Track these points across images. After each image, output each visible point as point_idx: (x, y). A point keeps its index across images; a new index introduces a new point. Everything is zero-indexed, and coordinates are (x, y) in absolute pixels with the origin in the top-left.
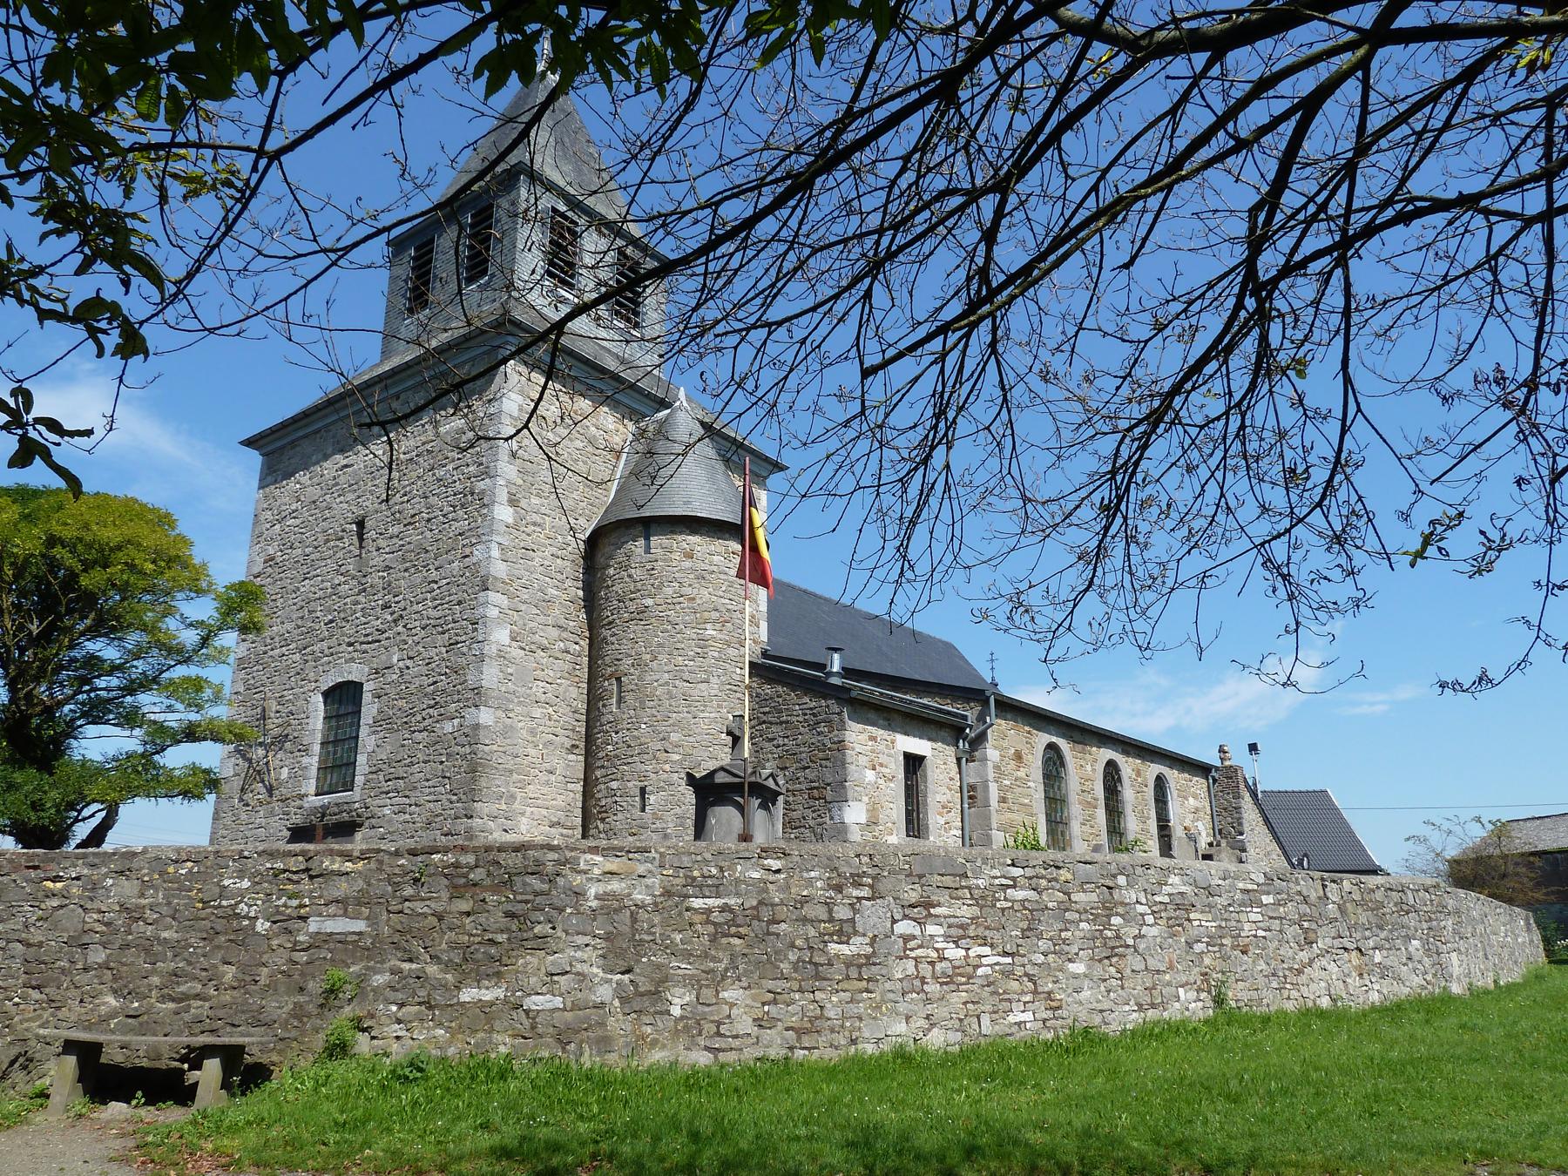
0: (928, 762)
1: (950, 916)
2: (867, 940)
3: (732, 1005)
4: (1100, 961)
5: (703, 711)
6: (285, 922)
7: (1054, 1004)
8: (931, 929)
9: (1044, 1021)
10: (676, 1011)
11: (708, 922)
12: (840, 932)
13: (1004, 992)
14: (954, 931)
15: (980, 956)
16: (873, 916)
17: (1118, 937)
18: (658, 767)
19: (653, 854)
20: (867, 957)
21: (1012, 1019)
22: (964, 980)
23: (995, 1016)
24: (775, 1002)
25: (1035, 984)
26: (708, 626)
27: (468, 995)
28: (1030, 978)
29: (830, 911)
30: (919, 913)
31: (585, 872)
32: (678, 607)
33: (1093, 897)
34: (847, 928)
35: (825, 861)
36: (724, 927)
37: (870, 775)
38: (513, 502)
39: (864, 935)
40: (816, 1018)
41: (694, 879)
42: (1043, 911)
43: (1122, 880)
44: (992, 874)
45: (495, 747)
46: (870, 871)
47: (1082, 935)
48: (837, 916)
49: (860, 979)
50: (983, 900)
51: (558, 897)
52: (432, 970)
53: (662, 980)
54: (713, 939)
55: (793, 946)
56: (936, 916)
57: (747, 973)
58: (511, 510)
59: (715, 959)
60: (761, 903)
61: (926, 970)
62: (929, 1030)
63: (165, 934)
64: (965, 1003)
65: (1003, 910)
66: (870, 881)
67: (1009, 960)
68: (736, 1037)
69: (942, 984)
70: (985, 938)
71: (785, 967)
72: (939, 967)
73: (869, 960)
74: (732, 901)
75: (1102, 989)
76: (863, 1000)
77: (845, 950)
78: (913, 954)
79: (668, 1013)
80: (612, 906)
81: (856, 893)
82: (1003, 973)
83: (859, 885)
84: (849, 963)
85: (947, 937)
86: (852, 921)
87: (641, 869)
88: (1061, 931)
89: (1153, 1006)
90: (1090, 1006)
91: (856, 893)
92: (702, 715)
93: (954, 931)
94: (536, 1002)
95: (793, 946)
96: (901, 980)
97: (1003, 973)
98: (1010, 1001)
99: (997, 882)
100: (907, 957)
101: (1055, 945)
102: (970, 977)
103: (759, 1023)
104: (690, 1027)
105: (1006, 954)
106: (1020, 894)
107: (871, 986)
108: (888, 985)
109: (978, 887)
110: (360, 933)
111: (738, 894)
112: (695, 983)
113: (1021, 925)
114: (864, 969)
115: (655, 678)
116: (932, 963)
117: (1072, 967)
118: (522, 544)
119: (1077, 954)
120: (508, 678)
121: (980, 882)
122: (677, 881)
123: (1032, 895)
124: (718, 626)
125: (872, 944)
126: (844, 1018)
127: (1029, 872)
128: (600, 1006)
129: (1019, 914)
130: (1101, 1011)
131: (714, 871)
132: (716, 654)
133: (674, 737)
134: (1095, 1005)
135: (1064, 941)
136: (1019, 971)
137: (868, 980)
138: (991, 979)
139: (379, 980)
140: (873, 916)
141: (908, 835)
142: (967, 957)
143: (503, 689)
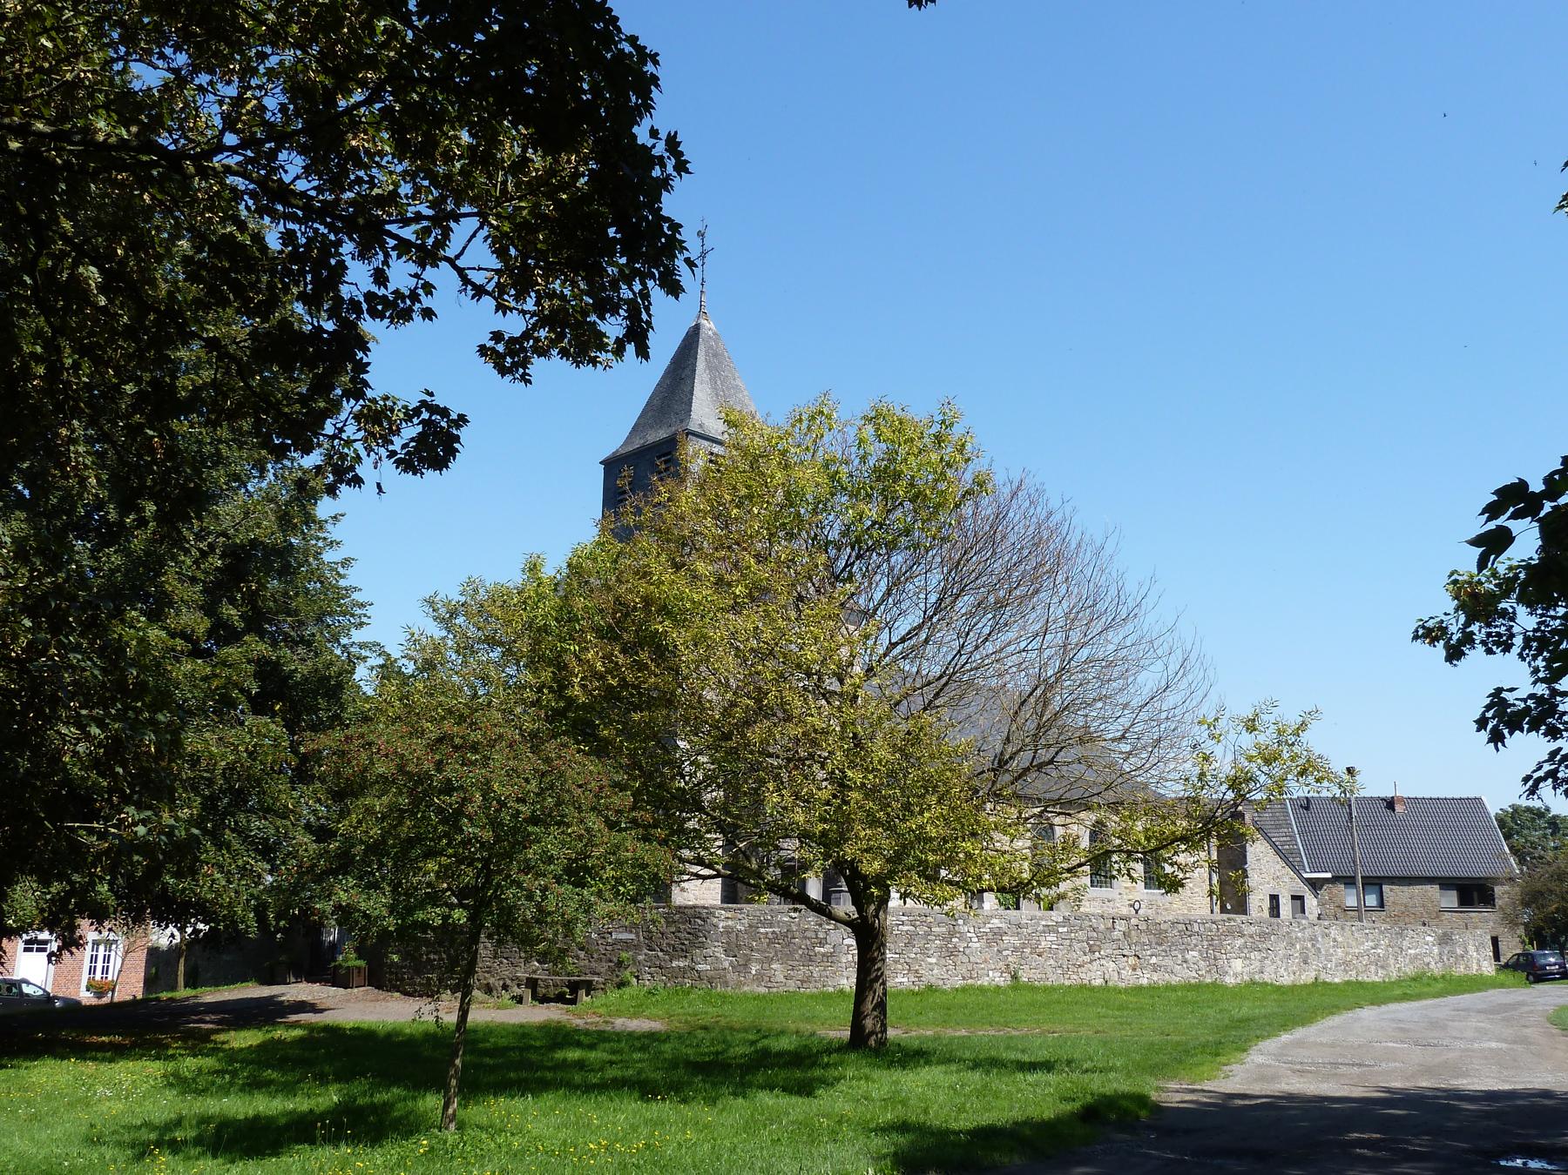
21: (897, 980)
43: (961, 922)
52: (660, 954)
53: (748, 960)
71: (797, 956)
77: (822, 949)
80: (728, 931)
84: (823, 955)
89: (971, 978)
94: (700, 967)
104: (759, 978)
106: (905, 928)
117: (929, 960)
123: (912, 928)
127: (911, 918)
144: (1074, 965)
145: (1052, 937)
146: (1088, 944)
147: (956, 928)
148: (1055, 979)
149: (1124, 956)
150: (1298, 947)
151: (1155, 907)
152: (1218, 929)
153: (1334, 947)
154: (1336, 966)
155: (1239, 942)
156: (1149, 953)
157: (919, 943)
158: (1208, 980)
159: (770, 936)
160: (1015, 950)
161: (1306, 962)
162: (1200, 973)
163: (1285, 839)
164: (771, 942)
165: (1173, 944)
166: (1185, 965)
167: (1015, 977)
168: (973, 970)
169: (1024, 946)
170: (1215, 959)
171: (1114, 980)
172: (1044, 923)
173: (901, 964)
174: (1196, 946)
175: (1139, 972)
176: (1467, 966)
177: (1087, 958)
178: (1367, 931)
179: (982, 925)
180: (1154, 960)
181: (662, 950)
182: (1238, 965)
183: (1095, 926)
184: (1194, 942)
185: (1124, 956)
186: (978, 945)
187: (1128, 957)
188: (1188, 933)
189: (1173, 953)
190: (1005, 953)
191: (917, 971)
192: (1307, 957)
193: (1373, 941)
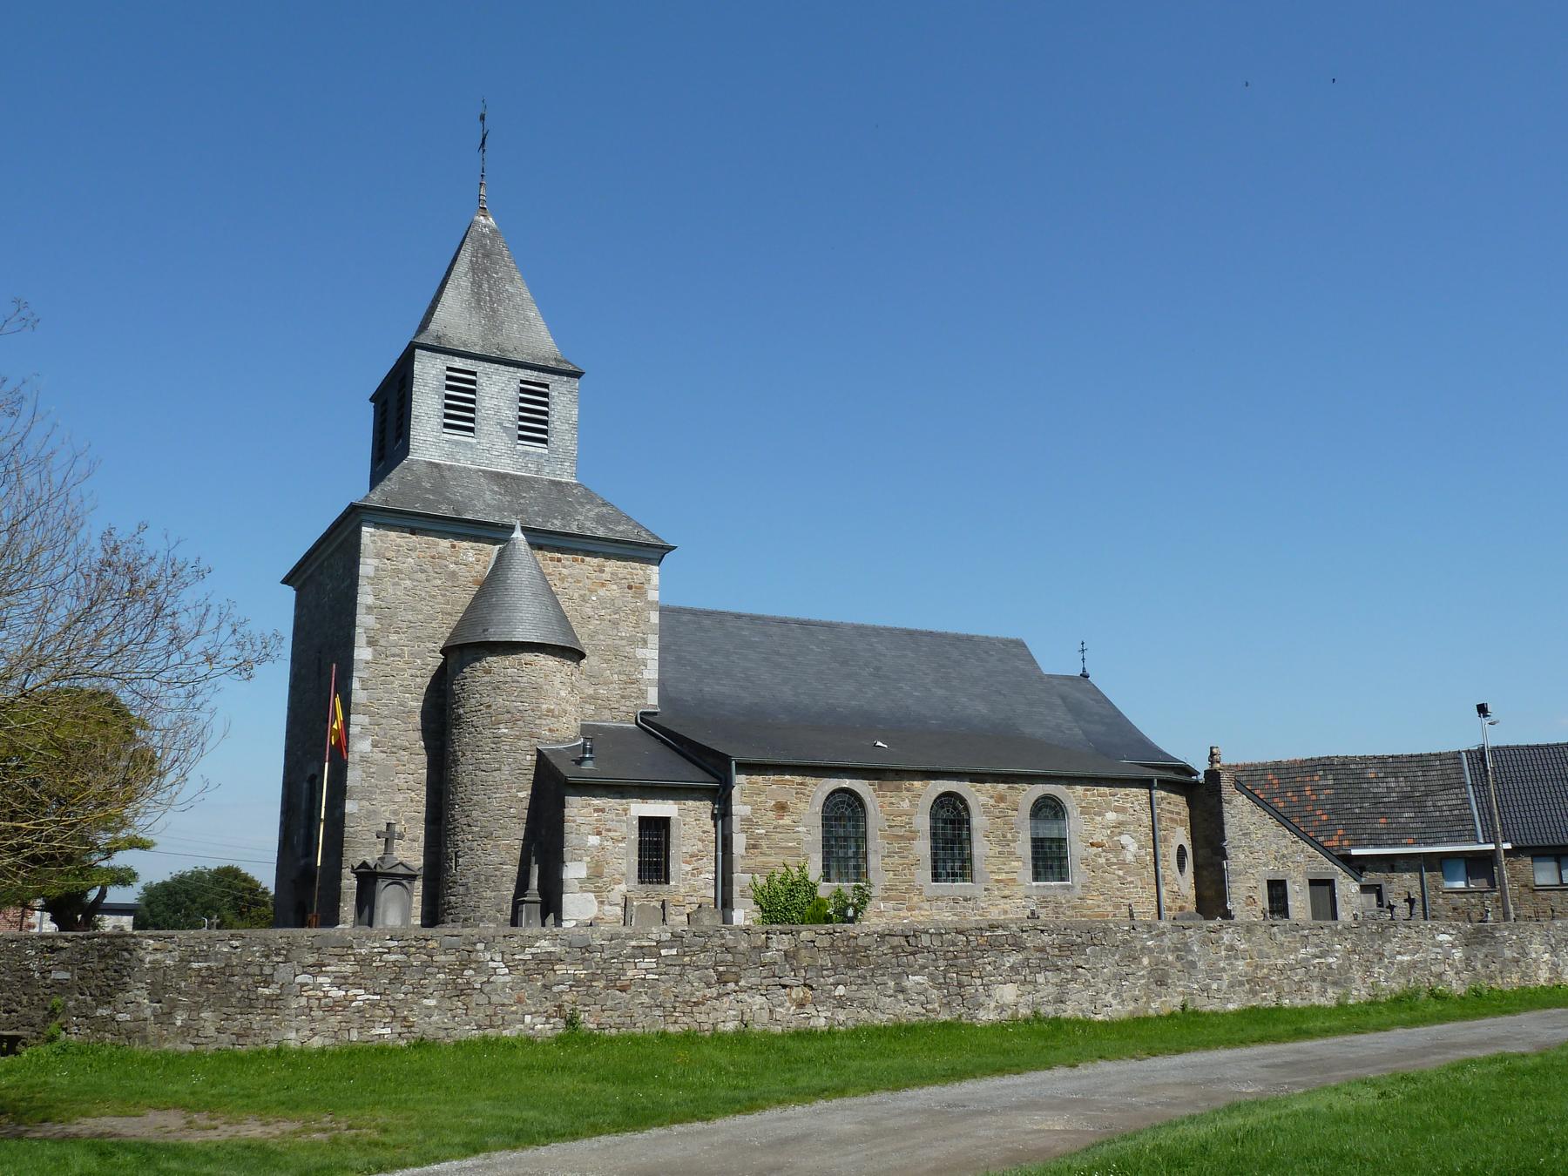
0: (672, 822)
1: (336, 972)
2: (279, 986)
3: (205, 1020)
4: (449, 998)
5: (495, 793)
6: (45, 973)
7: (408, 1024)
8: (320, 980)
9: (400, 1034)
10: (179, 1023)
11: (199, 975)
12: (265, 981)
13: (371, 1016)
14: (337, 981)
15: (356, 995)
16: (283, 973)
17: (468, 983)
18: (464, 837)
19: (176, 939)
20: (277, 995)
21: (374, 1032)
22: (340, 1009)
23: (360, 1030)
24: (227, 1019)
25: (394, 1012)
26: (501, 726)
27: (100, 1012)
28: (392, 1008)
29: (262, 970)
30: (313, 970)
31: (145, 949)
32: (479, 713)
33: (453, 958)
34: (269, 979)
35: (263, 941)
36: (205, 979)
37: (594, 840)
38: (371, 643)
39: (277, 983)
40: (248, 1029)
41: (195, 952)
42: (409, 967)
43: (480, 946)
44: (373, 945)
45: (360, 828)
46: (286, 946)
47: (437, 982)
48: (264, 972)
49: (272, 1008)
50: (363, 962)
51: (133, 963)
52: (89, 999)
53: (174, 1007)
54: (200, 985)
55: (240, 989)
56: (325, 972)
57: (214, 1004)
58: (370, 649)
59: (199, 996)
60: (226, 965)
61: (314, 1003)
62: (312, 1037)
63: (6, 979)
64: (340, 1022)
65: (377, 967)
66: (285, 952)
67: (378, 997)
68: (206, 1037)
69: (324, 1011)
70: (361, 984)
71: (234, 1001)
72: (323, 1001)
73: (278, 998)
74: (212, 964)
75: (449, 1015)
76: (272, 1020)
77: (267, 991)
78: (305, 994)
79: (174, 1024)
80: (155, 967)
81: (276, 959)
82: (371, 1005)
83: (278, 955)
84: (268, 998)
85: (332, 985)
86: (272, 975)
87: (170, 947)
88: (421, 979)
89: (492, 1026)
90: (437, 1026)
91: (276, 959)
92: (494, 796)
93: (337, 981)
94: (120, 1017)
95: (240, 989)
96: (296, 1009)
97: (371, 1005)
98: (374, 1022)
99: (376, 950)
100: (302, 996)
101: (414, 988)
102: (345, 1007)
103: (218, 1030)
104: (186, 1030)
105: (375, 994)
106: (392, 957)
107: (278, 1012)
108: (287, 1012)
109: (361, 954)
110: (67, 980)
111: (216, 961)
112: (189, 1009)
113: (389, 976)
114: (274, 1002)
115: (463, 769)
116: (319, 999)
117: (426, 1002)
118: (381, 674)
119: (431, 994)
120: (371, 775)
121: (362, 951)
122: (187, 953)
123: (402, 957)
124: (509, 725)
125: (280, 989)
126: (262, 1029)
127: (402, 943)
128: (145, 1019)
129: (389, 970)
130: (446, 1029)
131: (205, 948)
132: (507, 748)
133: (474, 814)
134: (441, 1025)
135: (422, 986)
136: (383, 1004)
137: (277, 1008)
138: (362, 1009)
139: (71, 1004)
140: (283, 973)
141: (642, 883)
142: (347, 995)
143: (366, 785)
144: (686, 1002)
145: (649, 962)
146: (716, 971)
147: (473, 956)
148: (647, 1023)
149: (784, 987)
150: (1145, 961)
151: (1052, 905)
152: (968, 942)
153: (1228, 957)
154: (1231, 986)
155: (1014, 958)
156: (831, 980)
157: (411, 979)
158: (945, 1016)
159: (204, 973)
160: (577, 982)
161: (1161, 982)
162: (929, 1007)
163: (1454, 802)
164: (204, 982)
165: (879, 966)
166: (901, 997)
167: (571, 1022)
168: (495, 1015)
169: (593, 977)
170: (960, 985)
171: (761, 1023)
172: (633, 943)
173: (383, 1009)
174: (923, 967)
175: (810, 1009)
176: (1524, 975)
177: (714, 992)
178: (1306, 932)
179: (517, 950)
180: (841, 990)
181: (91, 995)
182: (1008, 993)
183: (731, 944)
184: (921, 961)
185: (784, 987)
186: (508, 978)
187: (791, 987)
188: (909, 949)
189: (878, 980)
190: (555, 989)
191: (405, 1018)
192: (1166, 975)
193: (1317, 946)
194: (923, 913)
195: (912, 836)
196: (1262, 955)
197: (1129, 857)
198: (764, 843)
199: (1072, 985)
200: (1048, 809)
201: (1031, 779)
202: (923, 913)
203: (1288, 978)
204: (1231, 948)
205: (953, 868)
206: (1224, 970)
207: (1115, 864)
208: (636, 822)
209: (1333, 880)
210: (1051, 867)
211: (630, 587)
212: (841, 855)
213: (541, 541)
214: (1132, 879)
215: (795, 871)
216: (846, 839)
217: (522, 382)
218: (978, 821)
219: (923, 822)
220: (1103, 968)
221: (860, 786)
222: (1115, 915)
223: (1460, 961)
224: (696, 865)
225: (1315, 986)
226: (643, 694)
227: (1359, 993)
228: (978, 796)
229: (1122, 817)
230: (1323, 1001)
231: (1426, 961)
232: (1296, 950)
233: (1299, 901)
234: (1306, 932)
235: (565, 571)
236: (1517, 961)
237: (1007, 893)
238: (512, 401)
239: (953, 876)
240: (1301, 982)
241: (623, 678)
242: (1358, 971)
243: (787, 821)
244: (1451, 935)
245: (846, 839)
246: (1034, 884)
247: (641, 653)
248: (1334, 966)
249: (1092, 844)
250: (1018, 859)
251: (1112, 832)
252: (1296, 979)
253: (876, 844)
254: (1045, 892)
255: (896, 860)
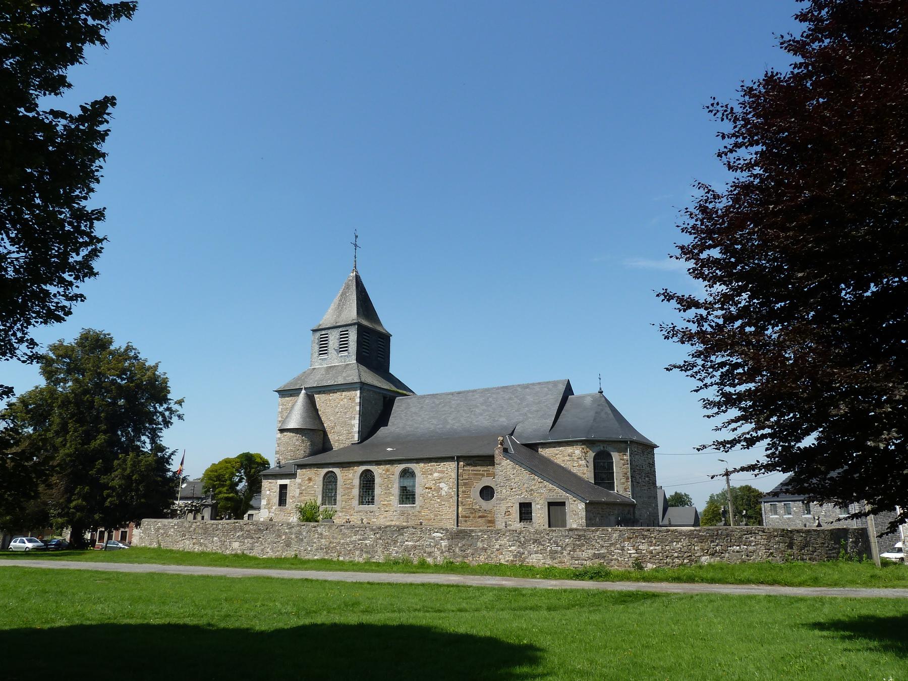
20: (838, 401)
37: (268, 492)
150: (284, 537)
178: (358, 529)
182: (236, 545)
194: (354, 517)
195: (353, 487)
196: (333, 537)
197: (443, 493)
198: (304, 492)
199: (256, 544)
200: (407, 474)
201: (400, 461)
202: (354, 517)
203: (345, 548)
204: (321, 534)
205: (368, 499)
206: (315, 543)
207: (436, 496)
208: (278, 486)
209: (565, 502)
210: (409, 498)
211: (350, 399)
212: (330, 495)
213: (319, 390)
214: (444, 503)
215: (313, 501)
216: (332, 489)
217: (341, 332)
218: (378, 480)
219: (357, 482)
220: (268, 539)
221: (336, 470)
222: (434, 519)
223: (445, 547)
224: (293, 500)
225: (357, 553)
226: (353, 437)
227: (379, 558)
228: (377, 470)
229: (441, 475)
230: (361, 560)
231: (423, 545)
232: (351, 537)
233: (540, 514)
234: (358, 529)
235: (331, 398)
236: (486, 550)
237: (387, 509)
238: (338, 339)
239: (368, 503)
240: (351, 550)
241: (347, 432)
242: (380, 548)
243: (311, 484)
244: (442, 533)
245: (332, 489)
246: (399, 505)
247: (353, 422)
248: (368, 545)
249: (426, 488)
250: (393, 495)
251: (436, 482)
252: (349, 549)
253: (340, 491)
254: (403, 509)
255: (346, 497)
